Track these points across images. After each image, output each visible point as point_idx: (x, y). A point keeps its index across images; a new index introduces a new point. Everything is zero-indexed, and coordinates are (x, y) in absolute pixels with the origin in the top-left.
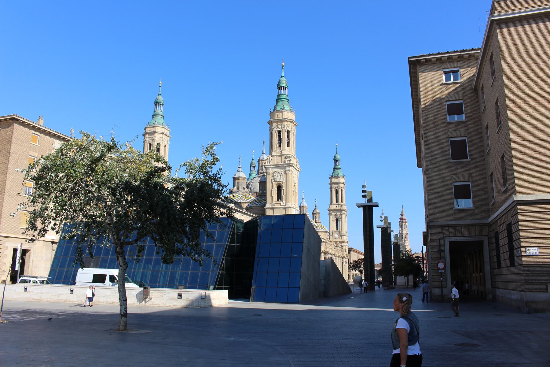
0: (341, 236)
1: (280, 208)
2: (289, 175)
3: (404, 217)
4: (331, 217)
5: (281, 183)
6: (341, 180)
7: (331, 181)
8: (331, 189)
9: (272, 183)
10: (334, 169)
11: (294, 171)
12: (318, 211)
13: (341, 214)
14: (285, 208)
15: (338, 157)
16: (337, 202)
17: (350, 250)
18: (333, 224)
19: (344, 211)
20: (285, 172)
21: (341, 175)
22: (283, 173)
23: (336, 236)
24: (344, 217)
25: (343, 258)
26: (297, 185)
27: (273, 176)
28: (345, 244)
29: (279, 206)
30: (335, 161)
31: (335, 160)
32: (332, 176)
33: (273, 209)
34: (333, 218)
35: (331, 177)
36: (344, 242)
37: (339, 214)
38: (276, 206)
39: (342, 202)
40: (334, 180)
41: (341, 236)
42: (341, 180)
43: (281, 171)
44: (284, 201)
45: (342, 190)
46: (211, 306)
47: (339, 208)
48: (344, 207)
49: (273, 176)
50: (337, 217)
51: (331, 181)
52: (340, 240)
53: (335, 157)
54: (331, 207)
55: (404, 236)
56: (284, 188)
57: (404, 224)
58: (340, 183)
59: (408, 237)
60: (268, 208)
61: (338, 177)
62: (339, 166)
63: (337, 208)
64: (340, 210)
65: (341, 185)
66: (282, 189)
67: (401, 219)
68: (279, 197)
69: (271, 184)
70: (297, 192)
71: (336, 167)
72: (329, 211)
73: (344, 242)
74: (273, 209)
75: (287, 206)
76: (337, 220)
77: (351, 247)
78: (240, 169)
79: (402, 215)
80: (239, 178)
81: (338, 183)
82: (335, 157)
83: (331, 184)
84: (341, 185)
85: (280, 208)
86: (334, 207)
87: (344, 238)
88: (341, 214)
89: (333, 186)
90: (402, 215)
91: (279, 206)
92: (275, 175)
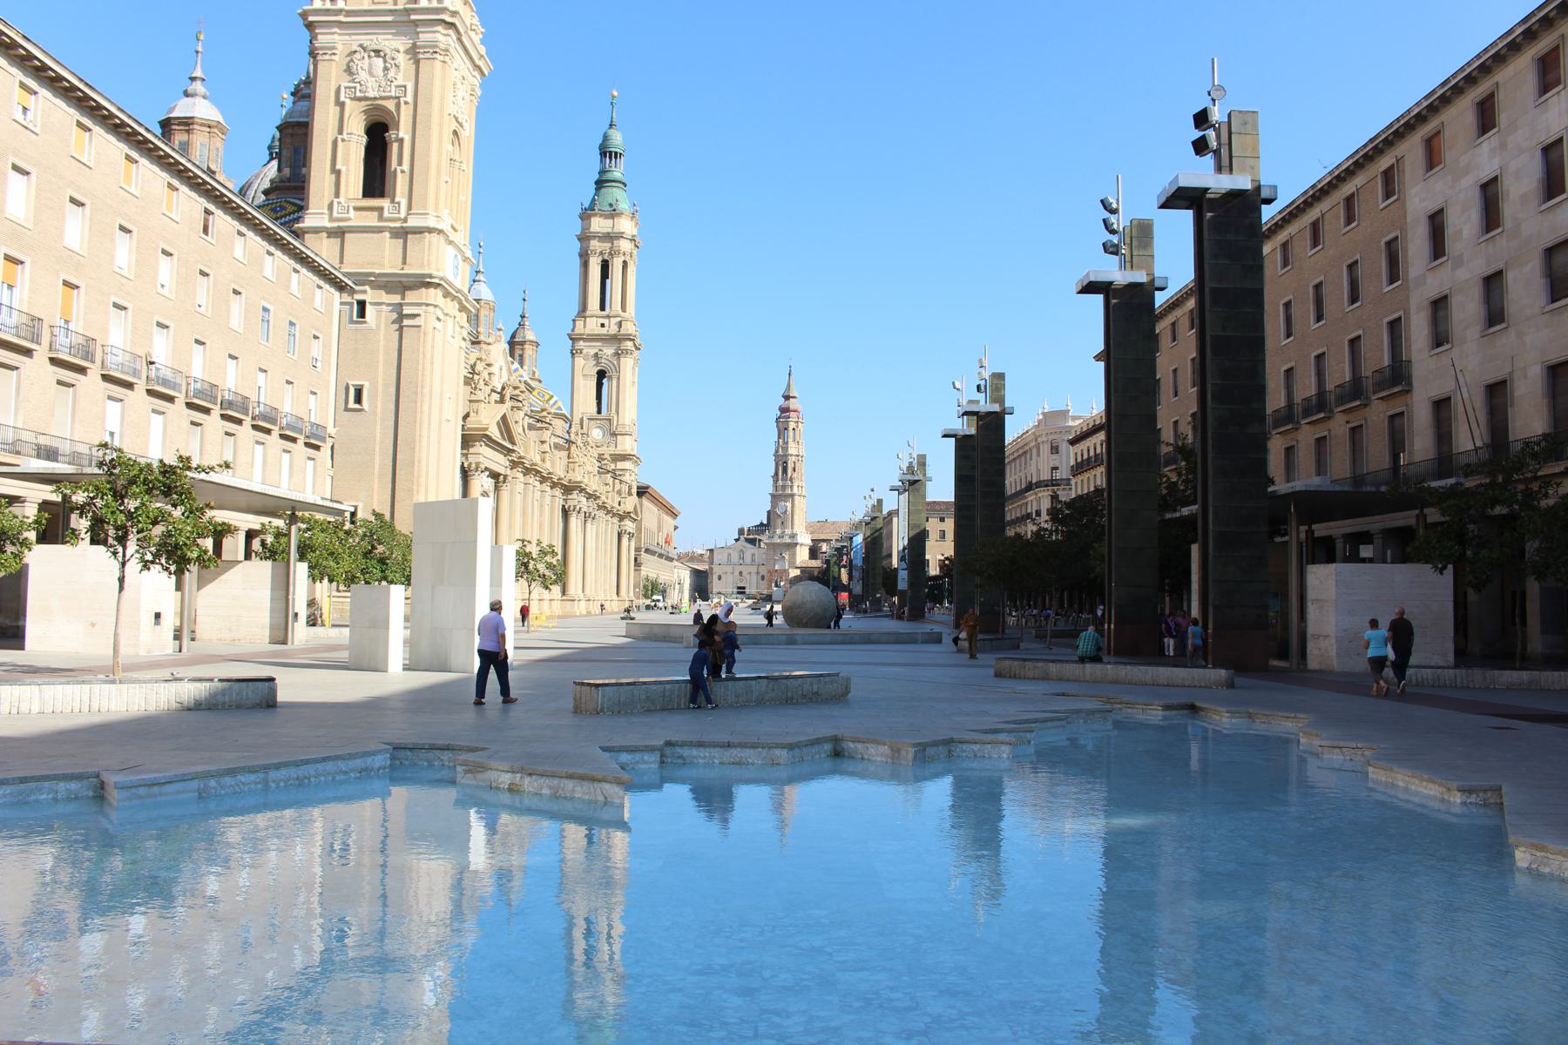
0: (614, 435)
1: (380, 230)
2: (434, 70)
3: (792, 404)
4: (579, 361)
5: (390, 105)
6: (626, 225)
7: (585, 228)
8: (584, 257)
9: (342, 105)
10: (600, 184)
11: (459, 61)
12: (530, 336)
13: (617, 355)
14: (402, 234)
15: (617, 139)
16: (602, 308)
17: (642, 492)
18: (587, 388)
19: (630, 344)
20: (413, 52)
21: (624, 206)
22: (402, 59)
23: (597, 434)
24: (627, 363)
25: (622, 518)
26: (468, 132)
27: (349, 70)
28: (627, 465)
29: (371, 220)
30: (603, 154)
31: (606, 152)
32: (592, 207)
33: (339, 233)
34: (586, 370)
35: (586, 215)
36: (624, 457)
37: (609, 351)
38: (356, 219)
39: (624, 310)
40: (598, 225)
41: (614, 435)
42: (626, 225)
43: (394, 44)
44: (401, 197)
45: (625, 263)
46: (1545, 436)
47: (613, 330)
48: (629, 328)
49: (349, 70)
50: (604, 364)
51: (585, 228)
52: (612, 450)
53: (606, 138)
54: (580, 324)
55: (790, 466)
56: (404, 132)
57: (792, 425)
58: (620, 236)
59: (801, 467)
60: (316, 231)
61: (613, 213)
62: (617, 175)
63: (604, 331)
64: (616, 339)
65: (624, 245)
66: (391, 135)
67: (784, 410)
68: (376, 181)
69: (334, 111)
70: (468, 167)
71: (609, 176)
72: (574, 339)
73: (624, 457)
74: (339, 233)
75: (413, 222)
76: (601, 375)
77: (645, 482)
78: (198, 87)
79: (787, 398)
80: (187, 123)
81: (610, 237)
82: (606, 138)
83: (584, 238)
84: (624, 245)
85: (380, 230)
86: (592, 326)
87: (627, 445)
88: (617, 355)
89: (595, 244)
90: (787, 398)
91: (371, 220)
92: (362, 63)
